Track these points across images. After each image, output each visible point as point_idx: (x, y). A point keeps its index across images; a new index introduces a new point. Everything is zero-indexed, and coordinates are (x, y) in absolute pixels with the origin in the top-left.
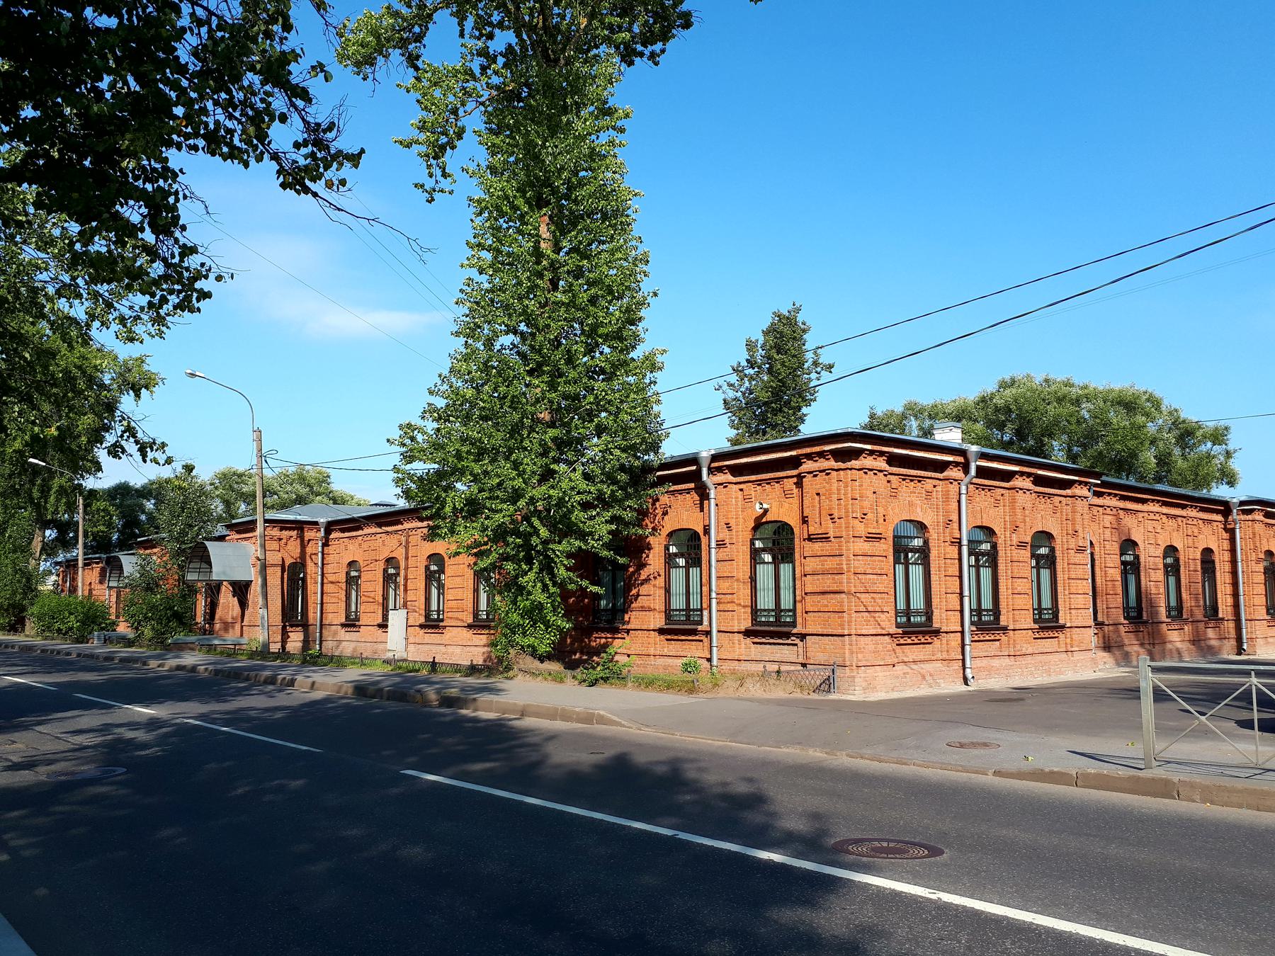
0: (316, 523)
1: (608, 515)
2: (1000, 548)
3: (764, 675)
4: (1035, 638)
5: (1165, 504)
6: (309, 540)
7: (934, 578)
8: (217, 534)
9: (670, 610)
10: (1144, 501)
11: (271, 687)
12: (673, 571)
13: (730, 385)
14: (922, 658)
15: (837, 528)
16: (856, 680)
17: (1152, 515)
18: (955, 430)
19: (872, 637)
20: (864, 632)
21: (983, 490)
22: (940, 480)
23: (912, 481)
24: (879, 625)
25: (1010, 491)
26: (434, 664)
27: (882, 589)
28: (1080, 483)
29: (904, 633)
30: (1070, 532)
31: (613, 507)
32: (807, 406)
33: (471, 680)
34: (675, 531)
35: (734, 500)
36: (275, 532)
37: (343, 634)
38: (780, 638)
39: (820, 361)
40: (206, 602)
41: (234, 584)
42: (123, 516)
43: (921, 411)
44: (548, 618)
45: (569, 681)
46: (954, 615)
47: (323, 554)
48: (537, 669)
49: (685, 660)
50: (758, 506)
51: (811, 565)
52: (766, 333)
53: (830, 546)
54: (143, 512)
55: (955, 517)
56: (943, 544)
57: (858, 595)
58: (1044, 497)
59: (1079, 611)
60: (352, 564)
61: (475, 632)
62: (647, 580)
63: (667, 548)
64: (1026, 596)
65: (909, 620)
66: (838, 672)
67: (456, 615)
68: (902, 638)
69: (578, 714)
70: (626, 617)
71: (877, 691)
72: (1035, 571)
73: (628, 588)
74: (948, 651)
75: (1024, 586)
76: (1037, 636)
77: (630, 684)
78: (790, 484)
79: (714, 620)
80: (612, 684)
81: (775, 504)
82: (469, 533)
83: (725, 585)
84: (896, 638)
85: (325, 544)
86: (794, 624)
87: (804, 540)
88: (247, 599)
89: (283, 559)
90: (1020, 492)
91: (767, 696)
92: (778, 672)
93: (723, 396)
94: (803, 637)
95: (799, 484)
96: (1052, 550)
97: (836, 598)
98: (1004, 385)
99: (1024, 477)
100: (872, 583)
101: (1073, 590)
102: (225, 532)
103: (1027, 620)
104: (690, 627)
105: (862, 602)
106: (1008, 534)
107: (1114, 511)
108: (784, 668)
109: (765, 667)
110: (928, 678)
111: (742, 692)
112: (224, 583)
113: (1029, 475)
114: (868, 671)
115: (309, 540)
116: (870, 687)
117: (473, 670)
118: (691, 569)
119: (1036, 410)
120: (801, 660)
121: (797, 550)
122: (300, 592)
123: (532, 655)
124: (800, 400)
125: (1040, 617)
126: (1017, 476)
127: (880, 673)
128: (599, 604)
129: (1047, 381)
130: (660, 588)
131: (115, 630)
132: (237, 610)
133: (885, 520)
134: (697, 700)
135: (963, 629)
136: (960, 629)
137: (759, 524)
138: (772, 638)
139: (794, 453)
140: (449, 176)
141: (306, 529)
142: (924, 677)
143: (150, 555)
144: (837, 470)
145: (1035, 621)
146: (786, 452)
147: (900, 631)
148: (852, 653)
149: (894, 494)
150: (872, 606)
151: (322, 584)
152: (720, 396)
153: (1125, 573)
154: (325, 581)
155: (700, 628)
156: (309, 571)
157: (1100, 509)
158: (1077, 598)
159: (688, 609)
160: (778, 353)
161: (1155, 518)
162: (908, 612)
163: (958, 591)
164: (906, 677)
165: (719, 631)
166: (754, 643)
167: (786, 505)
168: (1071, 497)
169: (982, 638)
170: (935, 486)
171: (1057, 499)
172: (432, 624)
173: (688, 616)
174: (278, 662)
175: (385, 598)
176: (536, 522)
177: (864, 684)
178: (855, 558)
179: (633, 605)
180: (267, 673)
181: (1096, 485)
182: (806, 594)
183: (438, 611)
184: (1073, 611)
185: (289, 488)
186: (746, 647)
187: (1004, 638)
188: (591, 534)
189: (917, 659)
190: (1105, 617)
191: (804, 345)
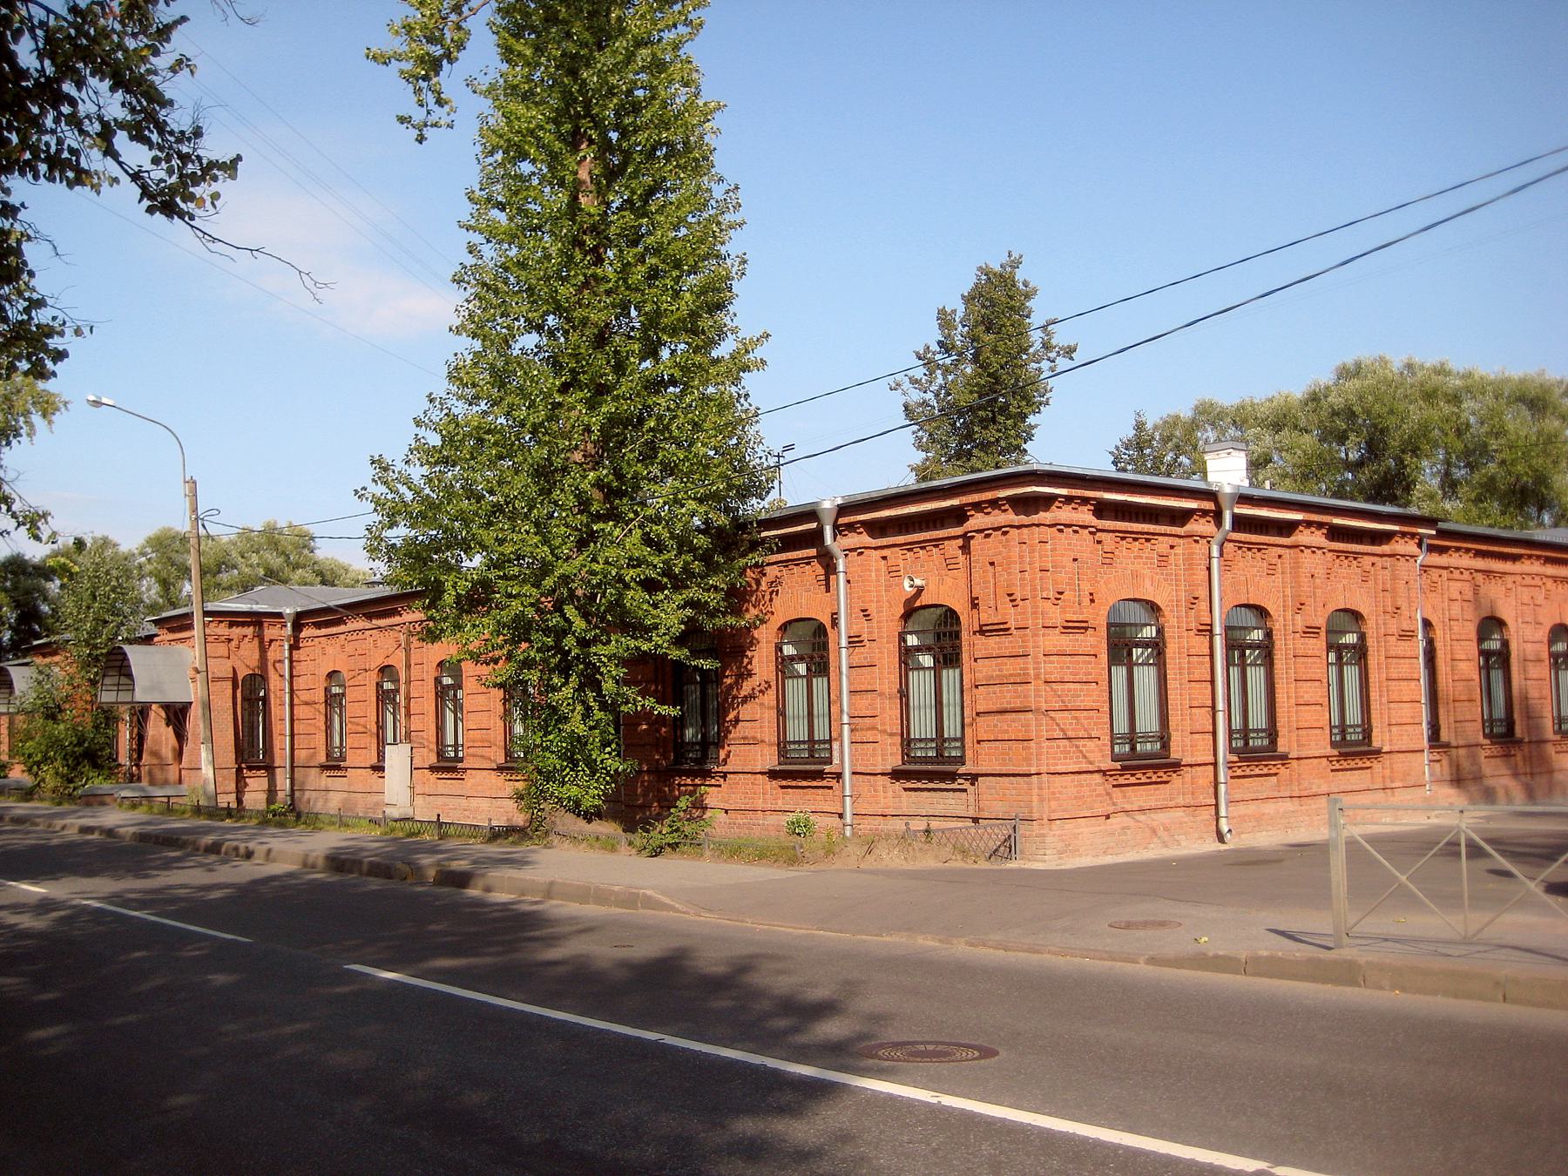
0: (279, 615)
1: (679, 598)
2: (1278, 637)
3: (904, 838)
4: (1332, 771)
5: (1548, 560)
6: (271, 641)
7: (1171, 684)
8: (143, 634)
9: (786, 742)
10: (1515, 558)
11: (213, 858)
12: (789, 683)
13: (914, 381)
14: (1153, 804)
15: (1020, 614)
16: (1048, 840)
17: (1528, 580)
18: (1235, 453)
19: (1073, 776)
20: (1060, 769)
21: (1249, 549)
22: (1180, 537)
23: (1135, 539)
24: (1085, 757)
25: (1292, 551)
26: (440, 824)
27: (1089, 705)
28: (1404, 534)
29: (1124, 768)
30: (1389, 609)
31: (687, 587)
32: (1034, 412)
33: (494, 849)
34: (790, 622)
35: (873, 574)
36: (223, 630)
37: (324, 780)
38: (942, 780)
39: (1054, 342)
40: (131, 733)
41: (166, 707)
42: (17, 605)
43: (1221, 415)
44: (594, 757)
45: (624, 848)
46: (1203, 740)
47: (291, 662)
48: (580, 833)
49: (791, 817)
50: (907, 583)
51: (985, 670)
52: (969, 299)
53: (1011, 642)
54: (45, 599)
55: (1202, 593)
56: (1186, 634)
57: (1052, 714)
58: (1347, 558)
59: (1404, 727)
60: (332, 675)
61: (909, 785)
62: (751, 697)
63: (779, 649)
64: (1318, 707)
65: (1133, 748)
66: (1023, 829)
67: (480, 751)
68: (1121, 775)
69: (617, 894)
70: (722, 754)
71: (1080, 856)
72: (1333, 670)
73: (722, 712)
74: (1193, 793)
75: (1312, 692)
76: (1337, 766)
77: (708, 853)
78: (953, 547)
79: (844, 757)
80: (683, 853)
81: (934, 580)
82: (480, 631)
83: (863, 703)
84: (1111, 776)
85: (294, 647)
86: (961, 760)
87: (974, 633)
88: (185, 730)
89: (234, 669)
90: (1306, 551)
91: (910, 866)
92: (928, 831)
93: (903, 400)
94: (973, 778)
95: (965, 549)
96: (1362, 637)
97: (1020, 720)
98: (1345, 373)
99: (1313, 529)
100: (1073, 696)
101: (1394, 697)
102: (153, 630)
103: (1320, 744)
104: (813, 767)
105: (1058, 725)
106: (1290, 613)
107: (1466, 575)
108: (935, 824)
109: (907, 824)
110: (1161, 832)
111: (869, 863)
112: (154, 707)
113: (1320, 525)
114: (1066, 826)
115: (271, 641)
116: (1066, 850)
117: (496, 835)
118: (814, 680)
119: (1391, 412)
120: (971, 813)
121: (965, 649)
122: (260, 719)
123: (574, 812)
124: (1024, 403)
125: (1344, 738)
126: (1301, 528)
127: (1085, 829)
128: (683, 735)
129: (1409, 366)
130: (770, 708)
131: (5, 777)
132: (173, 741)
133: (1092, 601)
134: (797, 874)
135: (1216, 760)
136: (1211, 759)
137: (910, 611)
138: (931, 781)
139: (955, 502)
140: (446, 103)
141: (266, 625)
142: (1154, 832)
143: (48, 666)
144: (1018, 527)
145: (1333, 744)
146: (945, 500)
147: (1118, 765)
148: (1041, 800)
149: (1108, 561)
150: (1073, 730)
151: (292, 705)
152: (898, 400)
153: (1486, 669)
154: (296, 701)
155: (827, 768)
156: (272, 688)
157: (1444, 573)
158: (1401, 709)
159: (811, 740)
160: (988, 330)
161: (1533, 583)
162: (1132, 737)
163: (1209, 703)
164: (1126, 834)
165: (854, 773)
166: (905, 789)
167: (949, 580)
168: (1390, 556)
169: (1248, 772)
170: (1172, 547)
171: (1367, 560)
172: (447, 765)
173: (812, 751)
174: (228, 823)
175: (381, 727)
176: (570, 611)
177: (1060, 846)
178: (1046, 659)
179: (731, 736)
180: (209, 839)
181: (1431, 537)
182: (978, 714)
183: (456, 745)
184: (1394, 729)
185: (255, 559)
186: (894, 796)
187: (1283, 770)
188: (656, 627)
189: (1146, 805)
190: (1453, 735)
191: (1028, 317)
